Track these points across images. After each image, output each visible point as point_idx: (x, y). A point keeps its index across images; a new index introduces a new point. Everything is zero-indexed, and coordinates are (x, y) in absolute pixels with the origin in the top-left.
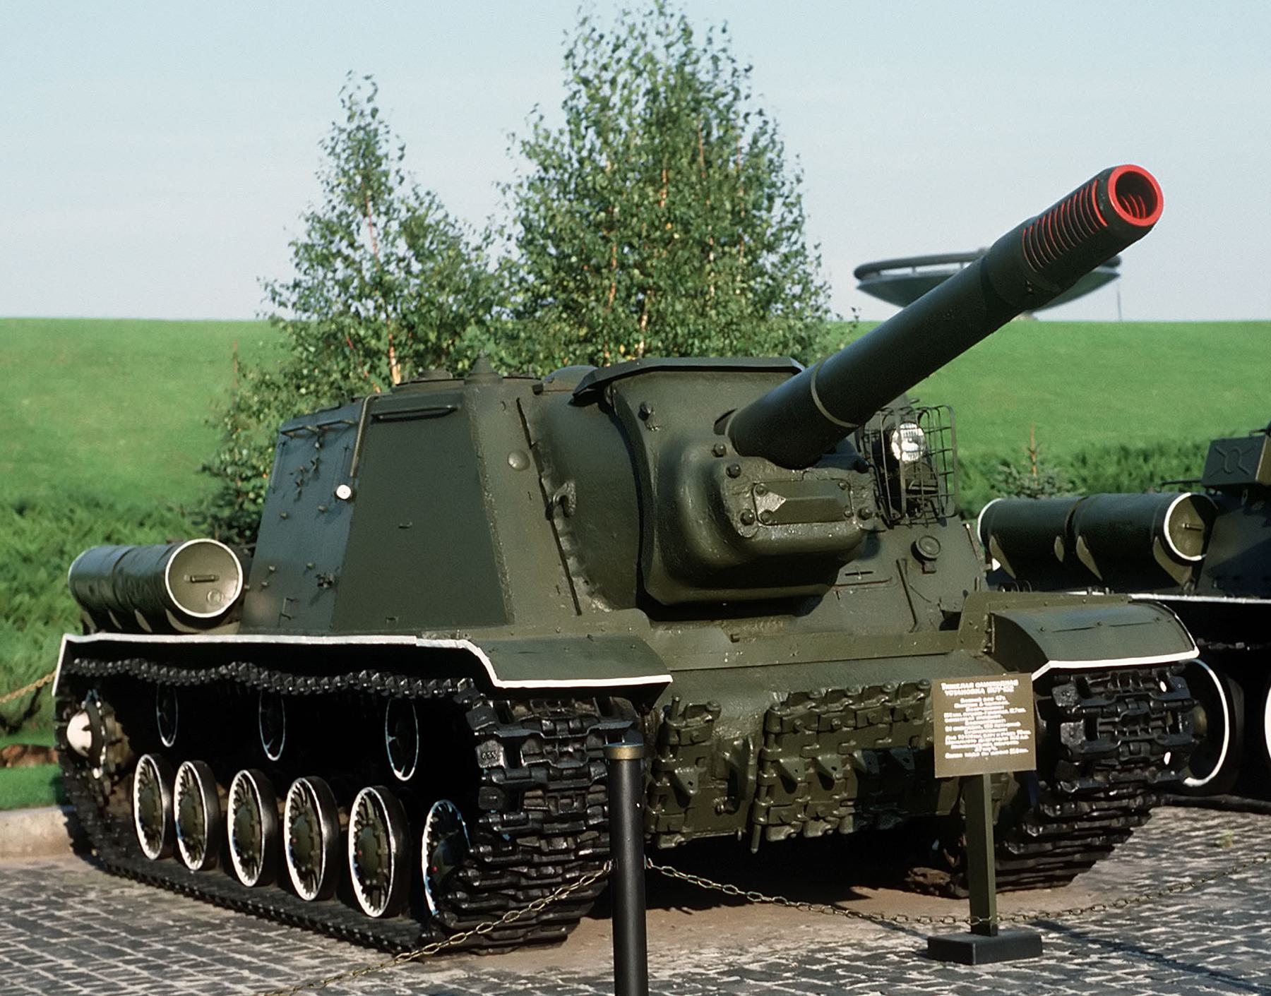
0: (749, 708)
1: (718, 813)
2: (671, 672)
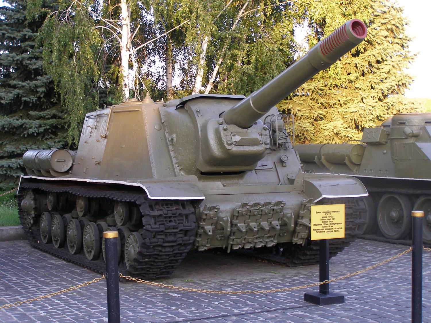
0: (148, 131)
1: (217, 239)
2: (205, 195)
